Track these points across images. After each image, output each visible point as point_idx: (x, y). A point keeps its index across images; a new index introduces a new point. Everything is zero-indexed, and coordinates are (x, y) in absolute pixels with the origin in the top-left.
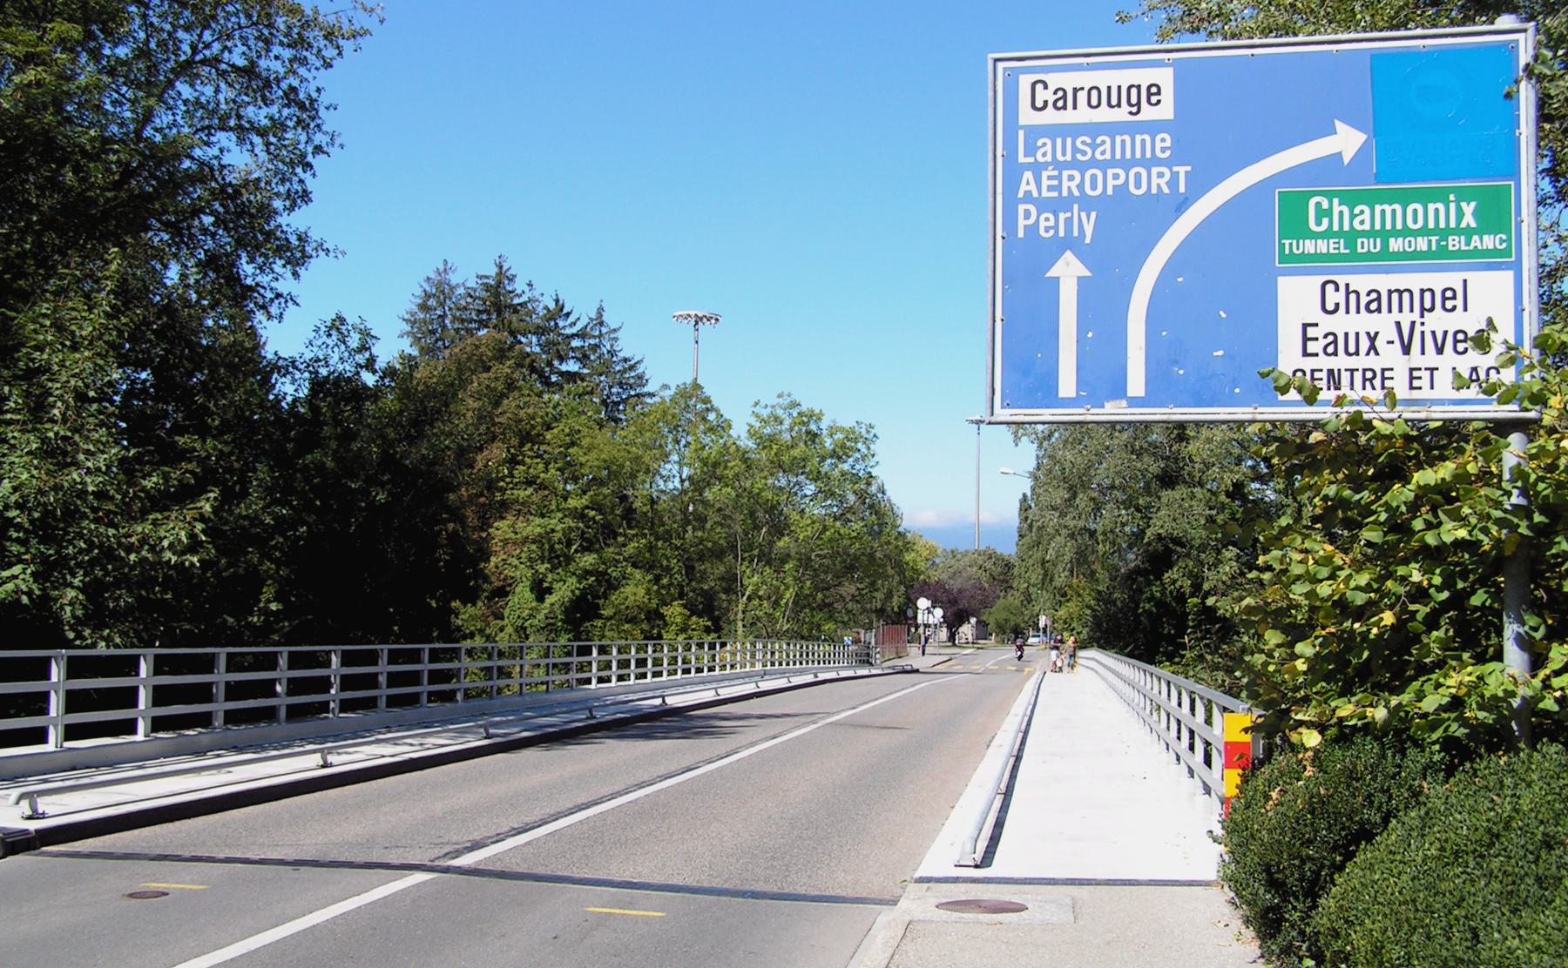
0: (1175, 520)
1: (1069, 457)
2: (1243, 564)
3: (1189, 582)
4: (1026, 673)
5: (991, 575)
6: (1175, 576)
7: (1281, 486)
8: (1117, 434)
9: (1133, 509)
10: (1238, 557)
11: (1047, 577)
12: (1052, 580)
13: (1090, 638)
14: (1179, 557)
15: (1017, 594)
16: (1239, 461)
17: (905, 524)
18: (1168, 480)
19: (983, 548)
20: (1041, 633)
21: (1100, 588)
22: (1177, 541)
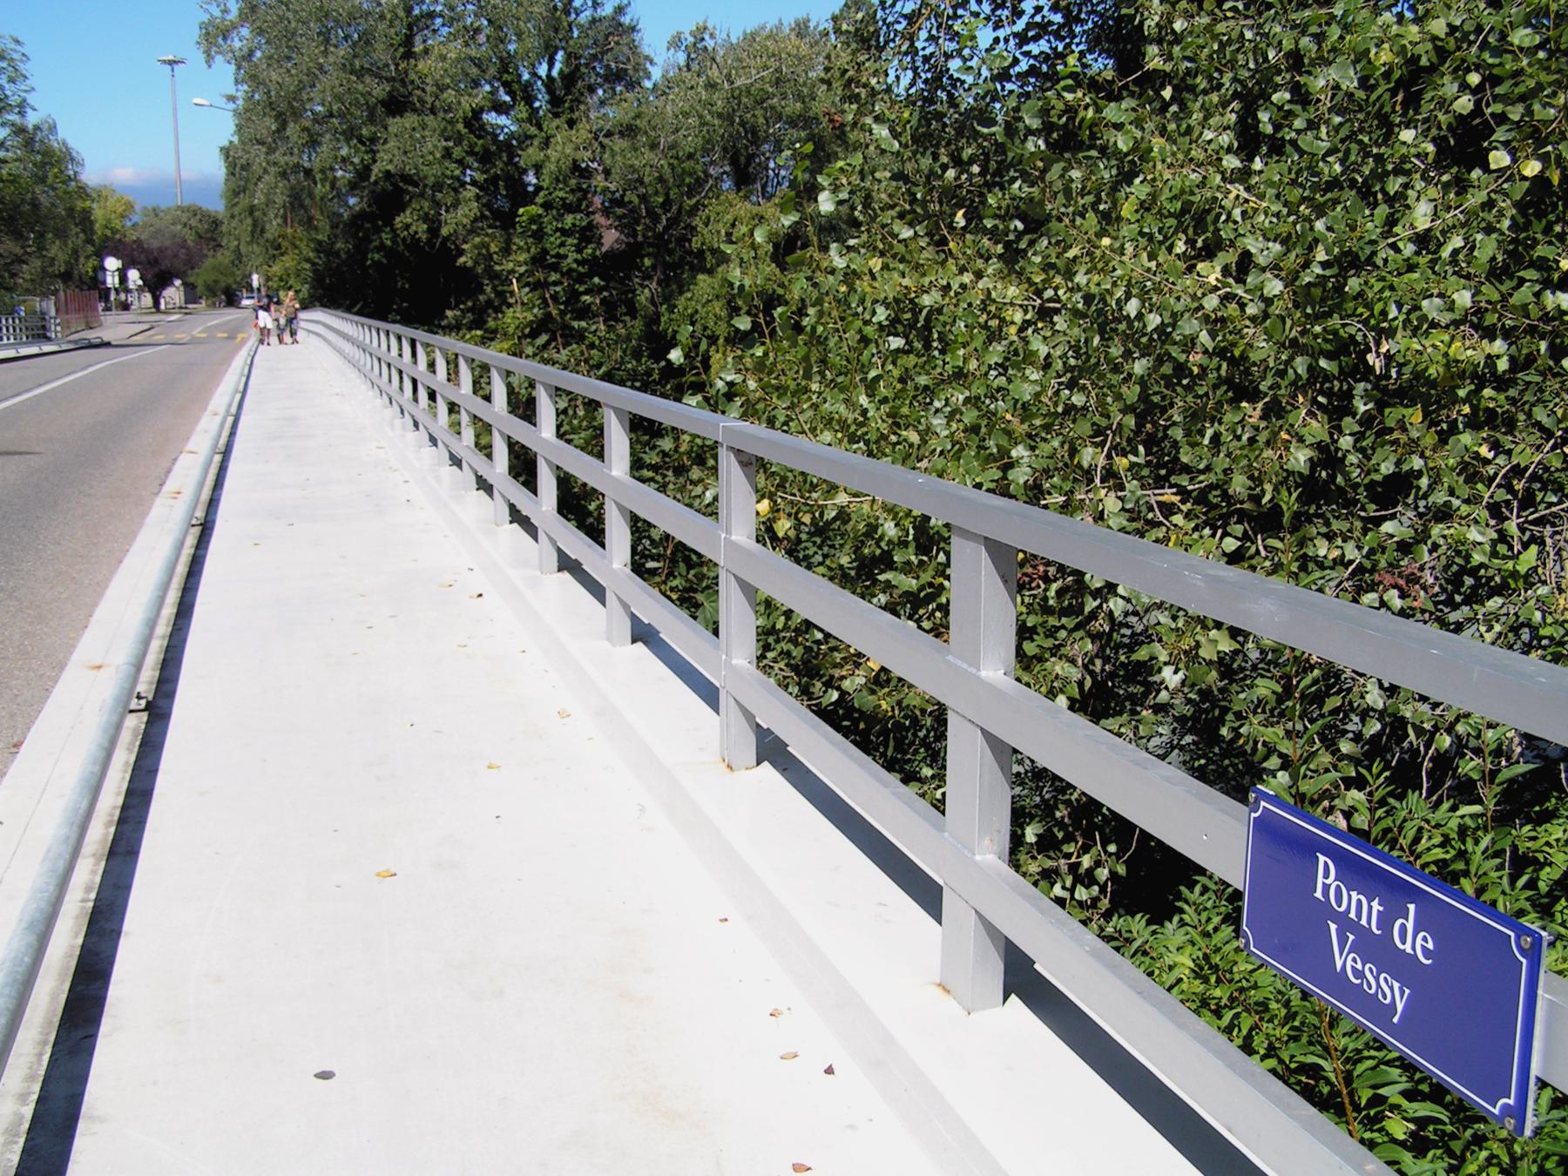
0: (405, 153)
1: (274, 76)
2: (484, 205)
3: (425, 226)
4: (239, 339)
5: (197, 233)
6: (409, 220)
7: (525, 115)
8: (332, 49)
9: (355, 141)
10: (478, 198)
11: (258, 229)
12: (263, 231)
13: (311, 296)
14: (411, 198)
15: (227, 253)
16: (476, 84)
17: (91, 174)
18: (396, 105)
19: (186, 204)
20: (255, 295)
21: (320, 237)
22: (407, 179)
